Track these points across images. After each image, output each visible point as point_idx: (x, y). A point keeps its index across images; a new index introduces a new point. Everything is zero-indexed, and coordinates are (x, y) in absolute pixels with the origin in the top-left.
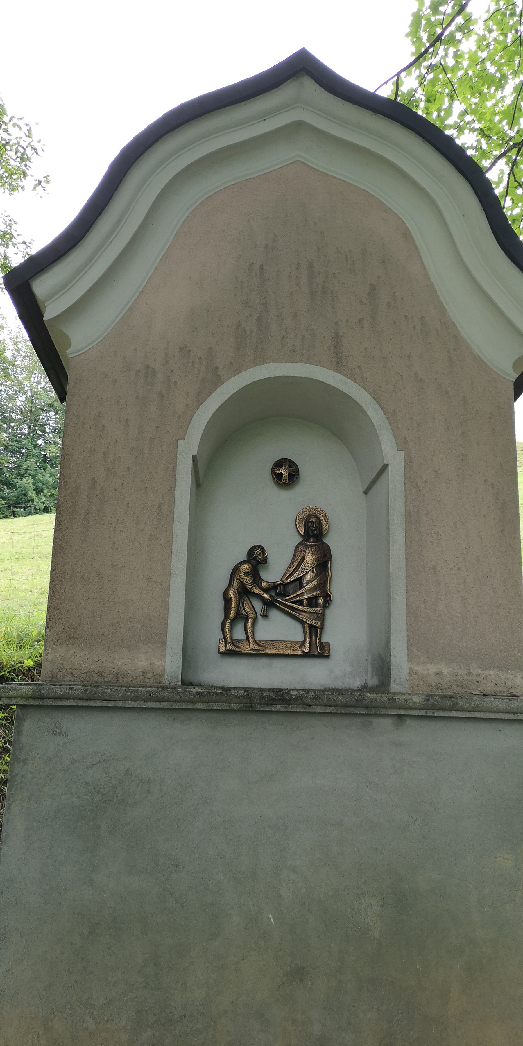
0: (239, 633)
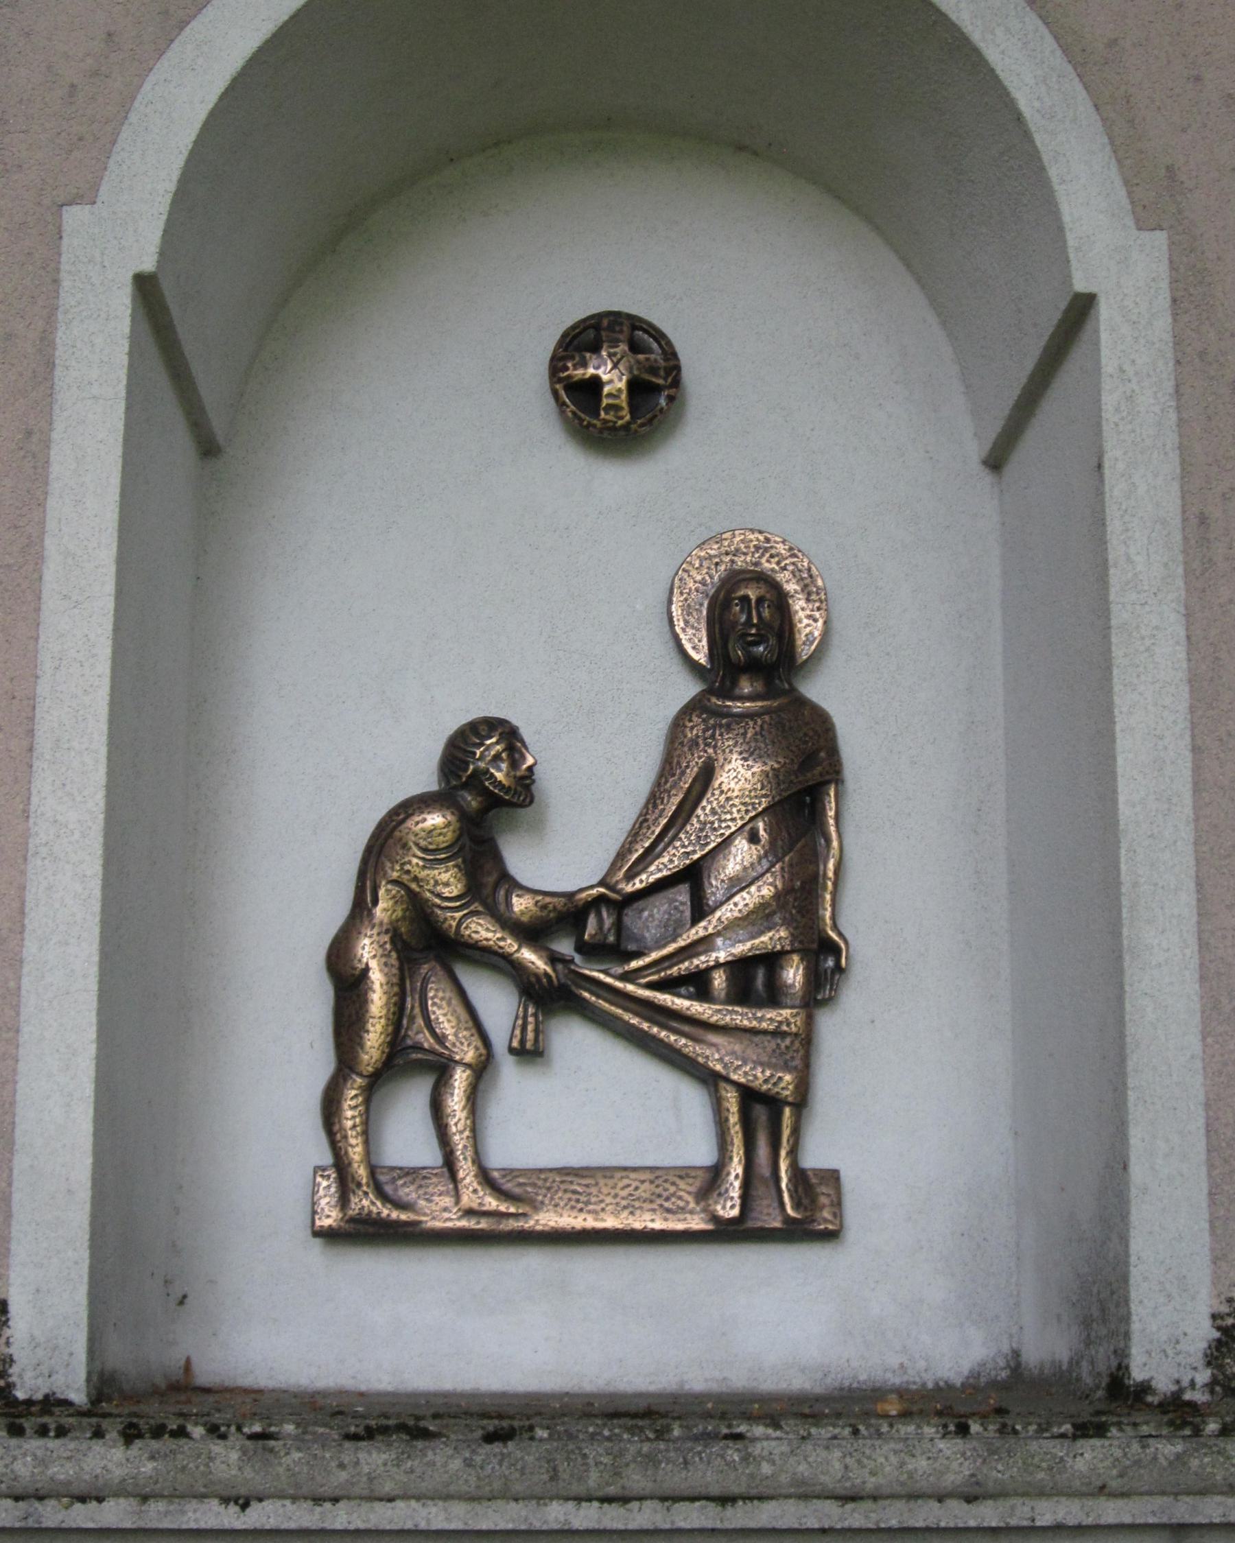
0: (406, 1136)
